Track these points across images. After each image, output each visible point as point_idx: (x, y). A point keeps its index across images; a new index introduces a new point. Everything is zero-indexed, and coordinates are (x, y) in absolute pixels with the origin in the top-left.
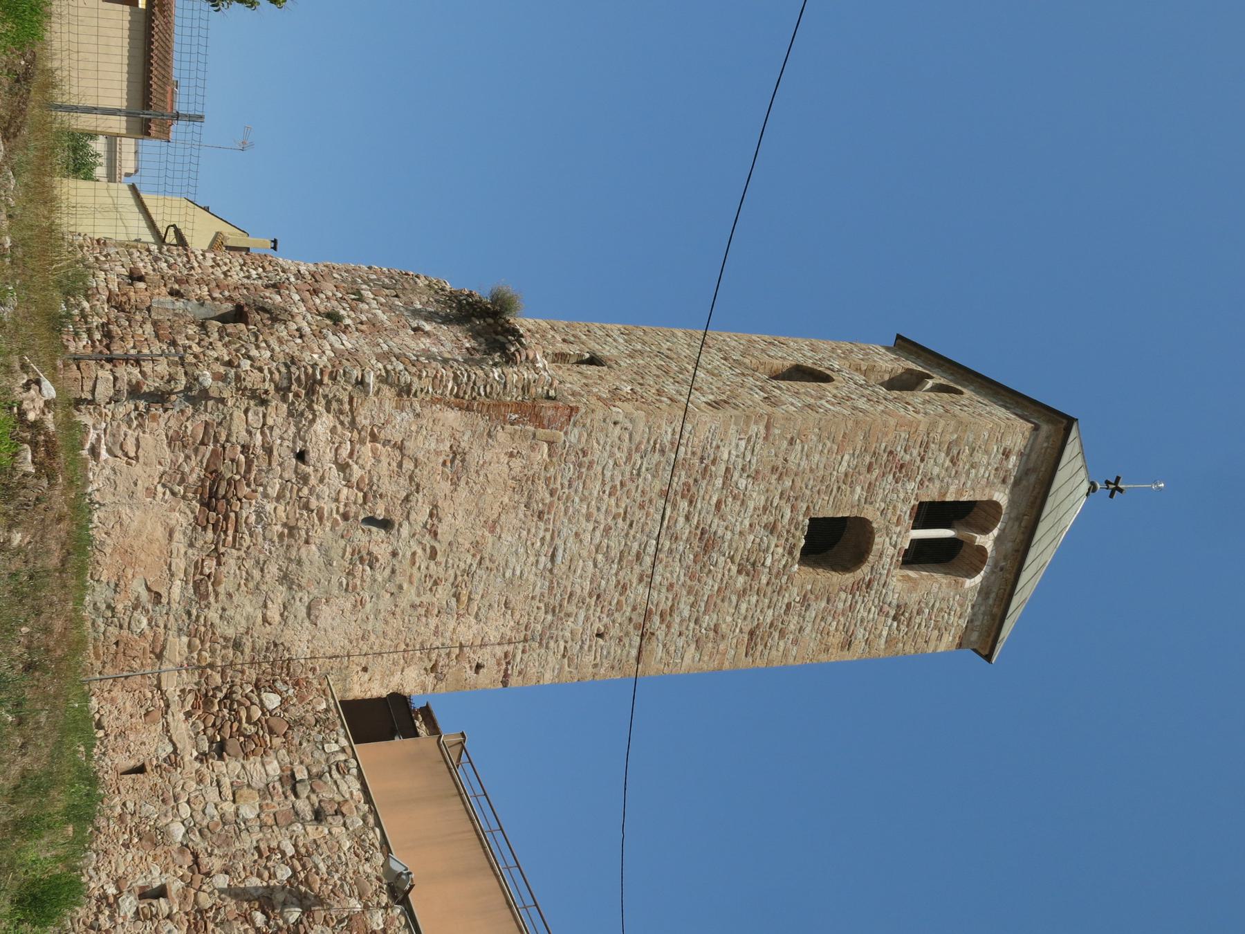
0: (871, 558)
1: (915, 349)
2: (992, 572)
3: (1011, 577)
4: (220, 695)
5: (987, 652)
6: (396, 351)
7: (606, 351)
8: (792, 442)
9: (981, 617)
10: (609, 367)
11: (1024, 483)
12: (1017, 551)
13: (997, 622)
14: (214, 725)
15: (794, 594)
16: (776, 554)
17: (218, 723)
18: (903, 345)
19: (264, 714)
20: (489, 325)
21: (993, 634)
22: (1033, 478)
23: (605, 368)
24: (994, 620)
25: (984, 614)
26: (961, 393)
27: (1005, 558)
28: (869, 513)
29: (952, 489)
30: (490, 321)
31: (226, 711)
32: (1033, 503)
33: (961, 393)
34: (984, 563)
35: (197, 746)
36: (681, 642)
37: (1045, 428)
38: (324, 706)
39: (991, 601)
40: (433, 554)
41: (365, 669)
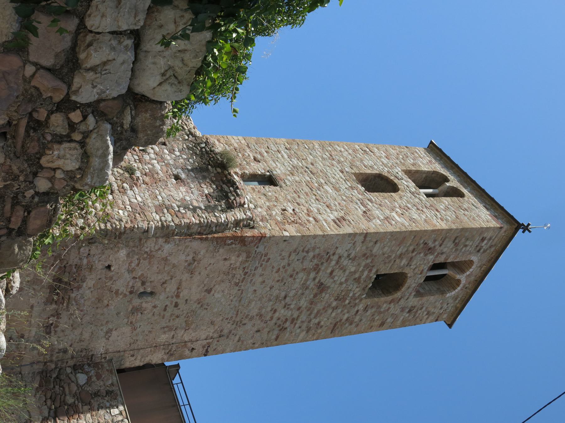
0: (403, 289)
1: (440, 153)
2: (461, 289)
3: (470, 292)
4: (54, 376)
5: (449, 323)
6: (167, 203)
7: (279, 171)
8: (376, 243)
9: (450, 308)
10: (281, 187)
11: (488, 251)
12: (476, 281)
13: (458, 311)
14: (51, 398)
15: (361, 307)
16: (356, 290)
17: (53, 397)
18: (434, 150)
19: (78, 388)
20: (218, 173)
21: (454, 316)
22: (493, 249)
23: (278, 188)
24: (456, 309)
25: (452, 307)
26: (462, 195)
27: (469, 283)
28: (406, 270)
29: (452, 257)
30: (219, 170)
31: (57, 387)
32: (490, 260)
33: (462, 195)
34: (458, 285)
35: (41, 413)
36: (298, 331)
37: (506, 227)
38: (110, 382)
39: (457, 301)
40: (176, 305)
41: (133, 356)
